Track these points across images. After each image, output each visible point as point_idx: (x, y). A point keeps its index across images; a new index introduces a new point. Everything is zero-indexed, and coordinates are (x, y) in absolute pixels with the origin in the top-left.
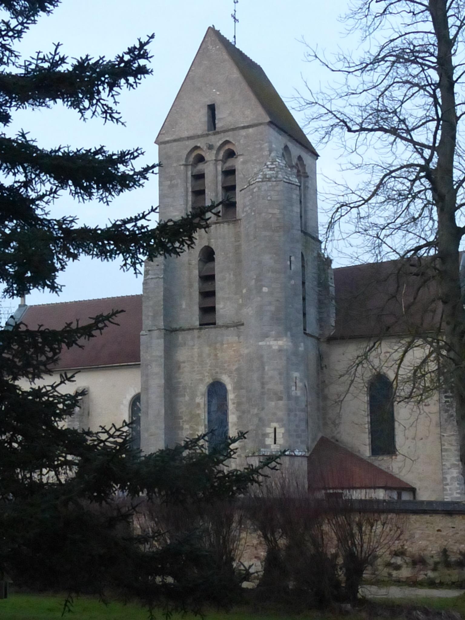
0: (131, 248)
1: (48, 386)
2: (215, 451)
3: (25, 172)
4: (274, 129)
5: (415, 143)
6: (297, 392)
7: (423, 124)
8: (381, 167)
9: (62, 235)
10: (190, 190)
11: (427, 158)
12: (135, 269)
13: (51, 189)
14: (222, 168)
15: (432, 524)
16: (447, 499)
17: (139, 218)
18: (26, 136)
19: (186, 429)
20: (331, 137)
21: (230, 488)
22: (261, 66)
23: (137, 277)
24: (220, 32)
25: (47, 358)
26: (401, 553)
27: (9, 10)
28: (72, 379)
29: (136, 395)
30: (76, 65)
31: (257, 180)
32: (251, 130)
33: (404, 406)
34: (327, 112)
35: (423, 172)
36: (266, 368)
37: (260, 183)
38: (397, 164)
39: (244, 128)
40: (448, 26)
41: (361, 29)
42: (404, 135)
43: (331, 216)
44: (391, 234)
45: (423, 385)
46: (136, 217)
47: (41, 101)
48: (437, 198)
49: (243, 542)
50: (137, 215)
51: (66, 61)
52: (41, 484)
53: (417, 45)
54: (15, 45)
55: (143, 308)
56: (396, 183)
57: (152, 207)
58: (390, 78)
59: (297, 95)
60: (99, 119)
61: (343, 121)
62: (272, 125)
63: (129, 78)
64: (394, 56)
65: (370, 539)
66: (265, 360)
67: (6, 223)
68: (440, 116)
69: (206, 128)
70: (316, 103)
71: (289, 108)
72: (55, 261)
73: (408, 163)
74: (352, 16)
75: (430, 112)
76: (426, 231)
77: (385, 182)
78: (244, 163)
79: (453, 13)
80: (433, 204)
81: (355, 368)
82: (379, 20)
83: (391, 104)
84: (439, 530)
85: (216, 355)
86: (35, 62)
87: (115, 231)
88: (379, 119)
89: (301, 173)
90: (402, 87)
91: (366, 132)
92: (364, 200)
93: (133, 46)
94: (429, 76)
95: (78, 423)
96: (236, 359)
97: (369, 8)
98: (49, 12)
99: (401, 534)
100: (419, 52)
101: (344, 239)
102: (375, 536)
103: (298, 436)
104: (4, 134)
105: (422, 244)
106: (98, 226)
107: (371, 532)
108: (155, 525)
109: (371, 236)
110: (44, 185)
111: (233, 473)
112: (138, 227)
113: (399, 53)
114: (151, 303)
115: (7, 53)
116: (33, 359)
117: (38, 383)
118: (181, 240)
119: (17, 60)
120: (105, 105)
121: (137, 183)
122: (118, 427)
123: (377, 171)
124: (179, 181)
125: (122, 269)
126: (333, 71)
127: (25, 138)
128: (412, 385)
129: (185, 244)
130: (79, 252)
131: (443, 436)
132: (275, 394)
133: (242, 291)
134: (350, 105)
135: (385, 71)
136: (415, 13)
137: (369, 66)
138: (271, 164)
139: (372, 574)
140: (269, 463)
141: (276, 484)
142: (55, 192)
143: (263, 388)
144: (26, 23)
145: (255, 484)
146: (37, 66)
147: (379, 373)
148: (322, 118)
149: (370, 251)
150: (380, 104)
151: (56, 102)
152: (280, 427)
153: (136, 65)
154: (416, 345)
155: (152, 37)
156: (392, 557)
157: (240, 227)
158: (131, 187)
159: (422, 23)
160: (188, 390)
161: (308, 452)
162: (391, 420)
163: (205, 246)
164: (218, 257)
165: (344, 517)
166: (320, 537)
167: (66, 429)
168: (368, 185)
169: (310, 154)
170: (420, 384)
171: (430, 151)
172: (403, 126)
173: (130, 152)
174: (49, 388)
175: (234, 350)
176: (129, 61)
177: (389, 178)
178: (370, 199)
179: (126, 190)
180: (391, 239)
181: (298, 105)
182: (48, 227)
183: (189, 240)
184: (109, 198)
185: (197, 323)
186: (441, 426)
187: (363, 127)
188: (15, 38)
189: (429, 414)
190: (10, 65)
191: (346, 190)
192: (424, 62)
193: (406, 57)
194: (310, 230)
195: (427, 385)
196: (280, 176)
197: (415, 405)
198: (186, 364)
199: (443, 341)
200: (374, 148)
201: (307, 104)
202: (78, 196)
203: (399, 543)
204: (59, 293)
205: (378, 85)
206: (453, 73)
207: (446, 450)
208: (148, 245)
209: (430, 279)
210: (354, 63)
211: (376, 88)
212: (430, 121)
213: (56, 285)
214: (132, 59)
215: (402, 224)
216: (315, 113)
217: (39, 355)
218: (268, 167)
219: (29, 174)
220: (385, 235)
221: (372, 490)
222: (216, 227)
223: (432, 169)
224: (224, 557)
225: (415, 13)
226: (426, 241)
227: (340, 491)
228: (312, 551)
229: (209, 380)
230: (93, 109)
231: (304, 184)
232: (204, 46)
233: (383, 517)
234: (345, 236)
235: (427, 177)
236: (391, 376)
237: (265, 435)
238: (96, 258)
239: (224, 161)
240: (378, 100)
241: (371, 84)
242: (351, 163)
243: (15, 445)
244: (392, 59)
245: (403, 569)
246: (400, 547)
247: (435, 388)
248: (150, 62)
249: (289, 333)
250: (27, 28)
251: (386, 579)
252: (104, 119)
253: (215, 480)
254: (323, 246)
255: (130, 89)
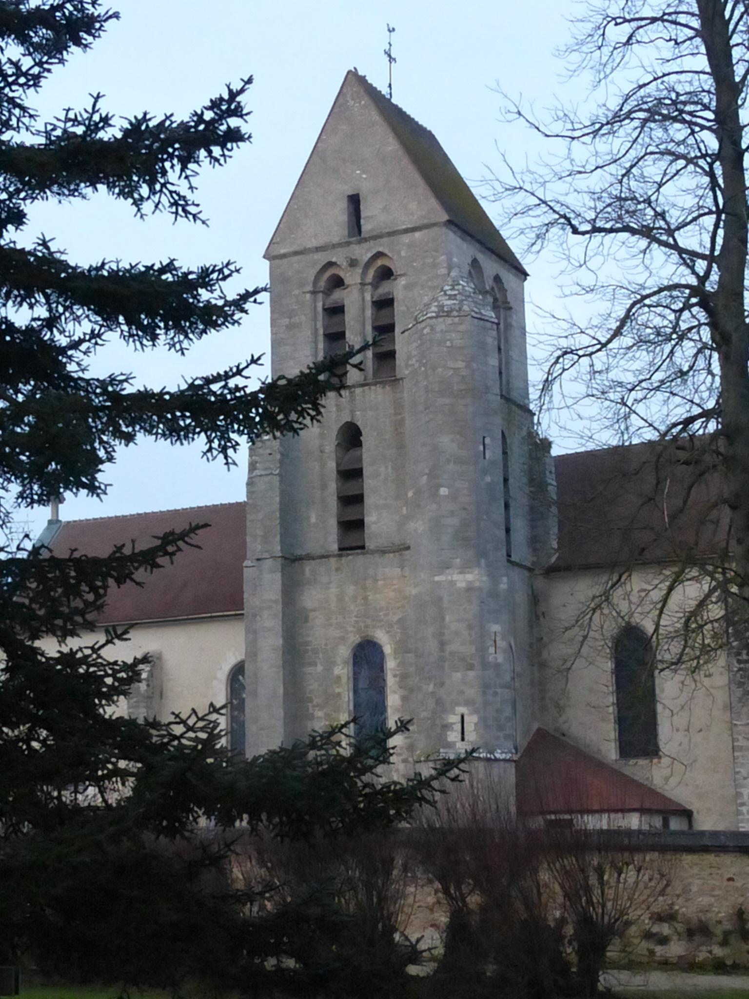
0: (219, 423)
1: (86, 648)
2: (359, 750)
3: (48, 303)
4: (455, 232)
5: (681, 251)
6: (497, 656)
7: (695, 219)
8: (628, 289)
9: (108, 404)
10: (321, 332)
11: (702, 274)
12: (226, 457)
13: (93, 331)
14: (372, 297)
15: (719, 869)
16: (743, 827)
17: (231, 374)
18: (49, 244)
19: (318, 718)
20: (546, 242)
21: (385, 811)
22: (434, 132)
23: (229, 470)
24: (367, 78)
25: (86, 603)
26: (669, 917)
27: (22, 45)
28: (125, 637)
29: (240, 663)
30: (127, 129)
31: (429, 315)
32: (417, 235)
33: (670, 676)
34: (538, 202)
35: (695, 297)
36: (447, 618)
37: (434, 320)
38: (652, 284)
39: (407, 231)
40: (731, 60)
41: (591, 68)
42: (664, 238)
43: (547, 370)
44: (645, 398)
45: (701, 642)
46: (226, 372)
47: (72, 187)
48: (718, 338)
49: (410, 900)
50: (228, 369)
51: (111, 122)
52: (76, 809)
53: (682, 92)
54: (30, 98)
55: (248, 523)
56: (652, 317)
57: (252, 356)
58: (639, 147)
59: (489, 176)
60: (166, 215)
61: (564, 217)
62: (453, 227)
63: (212, 148)
64: (645, 110)
65: (616, 894)
66: (445, 604)
67: (20, 385)
68: (721, 207)
69: (346, 232)
70: (521, 188)
71: (478, 197)
72: (97, 445)
73: (671, 283)
74: (577, 47)
75: (704, 201)
76: (701, 392)
77: (634, 314)
78: (407, 287)
79: (740, 41)
80: (712, 349)
81: (589, 616)
82: (621, 54)
83: (642, 188)
84: (730, 879)
85: (365, 598)
86: (62, 125)
87: (192, 396)
88: (623, 212)
89: (499, 303)
90: (659, 160)
91: (603, 234)
92: (600, 343)
93: (218, 96)
94: (703, 141)
95: (144, 710)
96: (399, 604)
97: (603, 34)
98: (86, 46)
99: (667, 885)
100: (685, 103)
101: (568, 407)
102: (625, 889)
103: (500, 728)
104: (14, 242)
105: (696, 413)
106: (164, 388)
107: (618, 882)
108: (267, 873)
109: (612, 401)
110: (79, 323)
111: (389, 787)
112: (229, 389)
113: (654, 105)
114: (260, 516)
115: (17, 111)
116: (62, 605)
117: (73, 643)
118: (299, 408)
119: (33, 123)
120: (175, 192)
121: (229, 319)
122: (200, 715)
123: (620, 296)
124: (303, 318)
125: (205, 457)
126: (547, 136)
127: (48, 248)
128: (683, 643)
129: (305, 415)
130: (134, 430)
131: (736, 725)
132: (463, 659)
133: (406, 494)
134: (575, 190)
135: (630, 135)
136: (679, 40)
137: (605, 127)
138: (451, 290)
139: (620, 951)
140: (448, 771)
141: (463, 806)
142: (99, 336)
143: (442, 650)
144: (47, 62)
145: (426, 806)
146: (65, 131)
147: (628, 623)
148: (530, 213)
149: (612, 426)
150: (624, 189)
151: (97, 190)
152: (470, 714)
153: (223, 128)
154: (688, 577)
155: (250, 81)
156: (653, 924)
157: (402, 392)
158: (219, 326)
159: (690, 56)
160: (321, 656)
161: (517, 753)
162: (650, 697)
163: (347, 423)
164: (368, 439)
165: (574, 859)
166: (535, 891)
167: (117, 719)
168: (606, 320)
169: (514, 271)
170: (695, 641)
171: (706, 262)
172: (662, 223)
173: (217, 268)
174: (88, 652)
175: (394, 590)
176: (213, 121)
177: (640, 308)
178: (610, 341)
179: (212, 330)
180: (644, 406)
181: (492, 192)
182: (87, 391)
183: (313, 410)
184: (185, 344)
185: (335, 547)
186: (731, 709)
187: (597, 225)
188: (29, 86)
189: (712, 690)
190: (21, 130)
191: (571, 328)
192: (694, 120)
193: (665, 112)
194: (515, 395)
195: (706, 642)
196: (466, 308)
197: (687, 675)
198: (317, 613)
199: (731, 570)
200: (615, 259)
201: (507, 190)
202: (134, 341)
203: (665, 901)
204: (102, 496)
205: (620, 159)
206: (741, 137)
207: (741, 748)
208: (247, 418)
209: (709, 469)
210: (581, 123)
211: (618, 162)
212: (705, 214)
213: (97, 484)
214: (217, 117)
215: (662, 382)
216: (519, 204)
217: (71, 597)
218: (445, 294)
219: (54, 305)
220: (635, 400)
221: (620, 815)
222: (364, 391)
223: (709, 291)
224: (380, 925)
225: (679, 40)
226: (702, 408)
227: (567, 817)
228: (524, 916)
229: (354, 639)
230: (156, 198)
231: (505, 319)
232: (341, 101)
233: (637, 858)
234: (570, 402)
235: (702, 304)
236: (649, 628)
237: (446, 727)
238: (163, 439)
239: (375, 285)
240: (621, 182)
241: (609, 157)
242: (578, 284)
243: (35, 745)
244: (642, 115)
245: (672, 943)
246: (667, 908)
247: (721, 647)
248: (246, 121)
249: (483, 561)
250: (49, 71)
251: (645, 960)
252: (174, 215)
253: (360, 799)
254: (536, 418)
255: (214, 167)
